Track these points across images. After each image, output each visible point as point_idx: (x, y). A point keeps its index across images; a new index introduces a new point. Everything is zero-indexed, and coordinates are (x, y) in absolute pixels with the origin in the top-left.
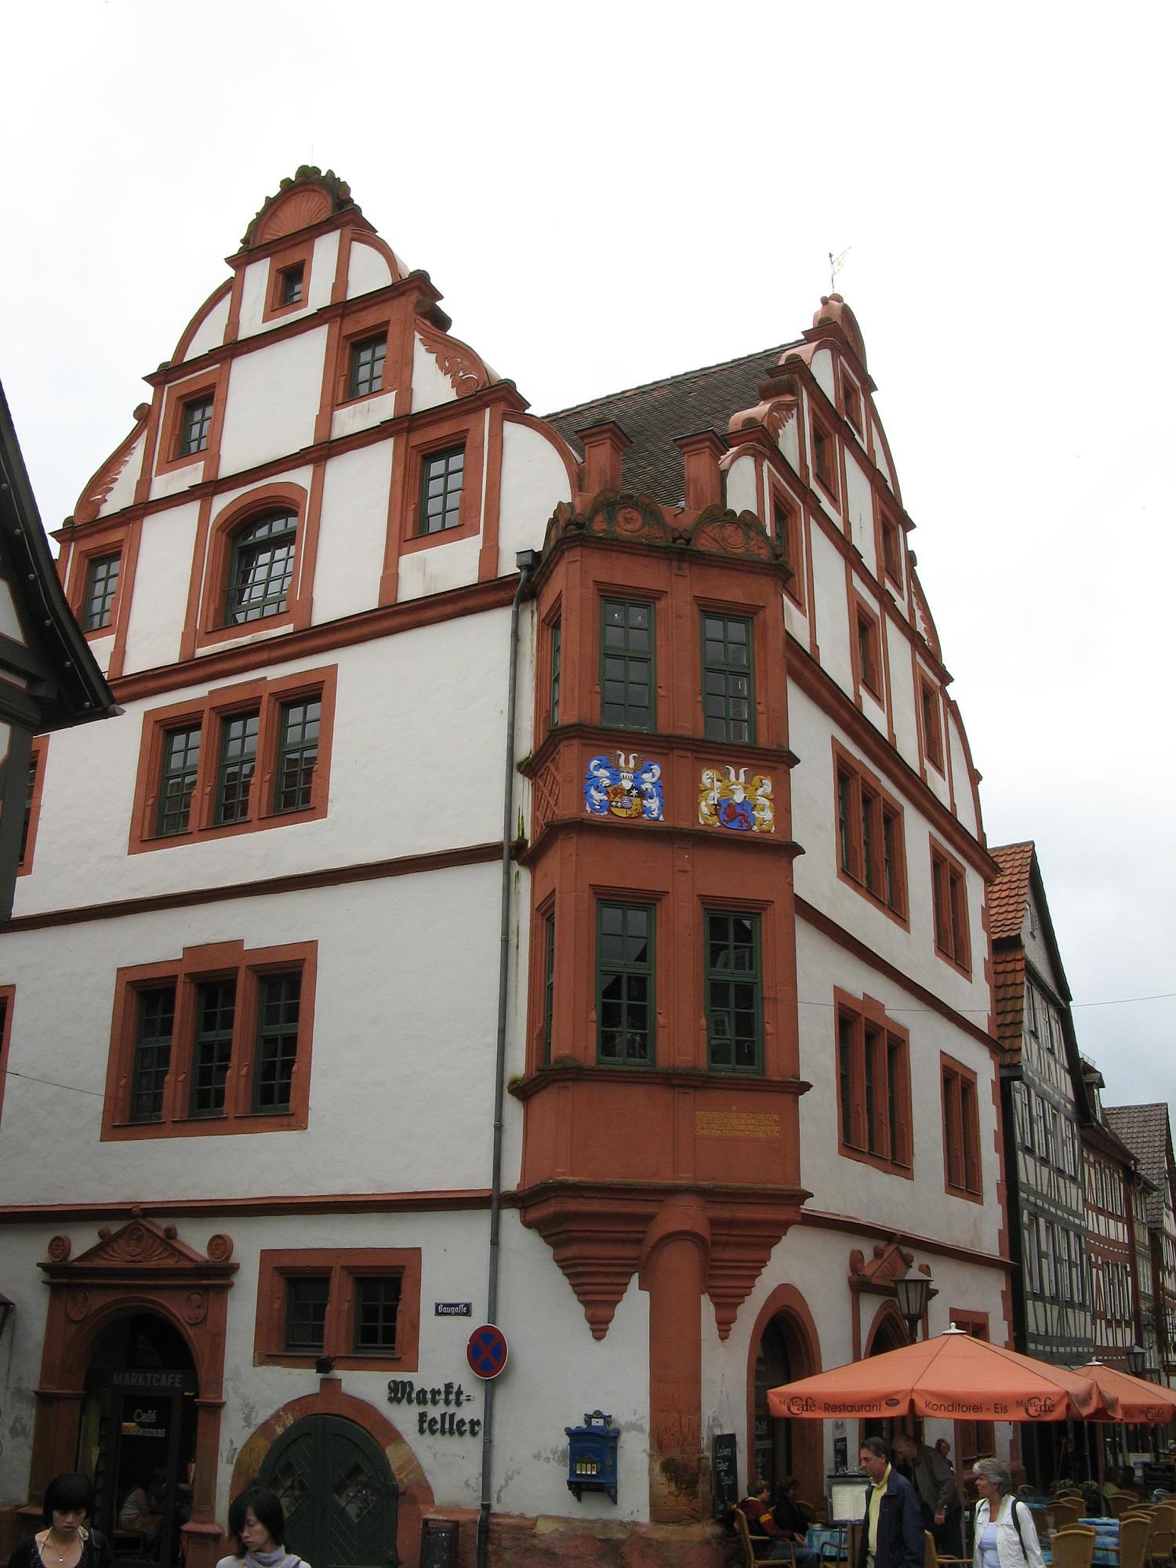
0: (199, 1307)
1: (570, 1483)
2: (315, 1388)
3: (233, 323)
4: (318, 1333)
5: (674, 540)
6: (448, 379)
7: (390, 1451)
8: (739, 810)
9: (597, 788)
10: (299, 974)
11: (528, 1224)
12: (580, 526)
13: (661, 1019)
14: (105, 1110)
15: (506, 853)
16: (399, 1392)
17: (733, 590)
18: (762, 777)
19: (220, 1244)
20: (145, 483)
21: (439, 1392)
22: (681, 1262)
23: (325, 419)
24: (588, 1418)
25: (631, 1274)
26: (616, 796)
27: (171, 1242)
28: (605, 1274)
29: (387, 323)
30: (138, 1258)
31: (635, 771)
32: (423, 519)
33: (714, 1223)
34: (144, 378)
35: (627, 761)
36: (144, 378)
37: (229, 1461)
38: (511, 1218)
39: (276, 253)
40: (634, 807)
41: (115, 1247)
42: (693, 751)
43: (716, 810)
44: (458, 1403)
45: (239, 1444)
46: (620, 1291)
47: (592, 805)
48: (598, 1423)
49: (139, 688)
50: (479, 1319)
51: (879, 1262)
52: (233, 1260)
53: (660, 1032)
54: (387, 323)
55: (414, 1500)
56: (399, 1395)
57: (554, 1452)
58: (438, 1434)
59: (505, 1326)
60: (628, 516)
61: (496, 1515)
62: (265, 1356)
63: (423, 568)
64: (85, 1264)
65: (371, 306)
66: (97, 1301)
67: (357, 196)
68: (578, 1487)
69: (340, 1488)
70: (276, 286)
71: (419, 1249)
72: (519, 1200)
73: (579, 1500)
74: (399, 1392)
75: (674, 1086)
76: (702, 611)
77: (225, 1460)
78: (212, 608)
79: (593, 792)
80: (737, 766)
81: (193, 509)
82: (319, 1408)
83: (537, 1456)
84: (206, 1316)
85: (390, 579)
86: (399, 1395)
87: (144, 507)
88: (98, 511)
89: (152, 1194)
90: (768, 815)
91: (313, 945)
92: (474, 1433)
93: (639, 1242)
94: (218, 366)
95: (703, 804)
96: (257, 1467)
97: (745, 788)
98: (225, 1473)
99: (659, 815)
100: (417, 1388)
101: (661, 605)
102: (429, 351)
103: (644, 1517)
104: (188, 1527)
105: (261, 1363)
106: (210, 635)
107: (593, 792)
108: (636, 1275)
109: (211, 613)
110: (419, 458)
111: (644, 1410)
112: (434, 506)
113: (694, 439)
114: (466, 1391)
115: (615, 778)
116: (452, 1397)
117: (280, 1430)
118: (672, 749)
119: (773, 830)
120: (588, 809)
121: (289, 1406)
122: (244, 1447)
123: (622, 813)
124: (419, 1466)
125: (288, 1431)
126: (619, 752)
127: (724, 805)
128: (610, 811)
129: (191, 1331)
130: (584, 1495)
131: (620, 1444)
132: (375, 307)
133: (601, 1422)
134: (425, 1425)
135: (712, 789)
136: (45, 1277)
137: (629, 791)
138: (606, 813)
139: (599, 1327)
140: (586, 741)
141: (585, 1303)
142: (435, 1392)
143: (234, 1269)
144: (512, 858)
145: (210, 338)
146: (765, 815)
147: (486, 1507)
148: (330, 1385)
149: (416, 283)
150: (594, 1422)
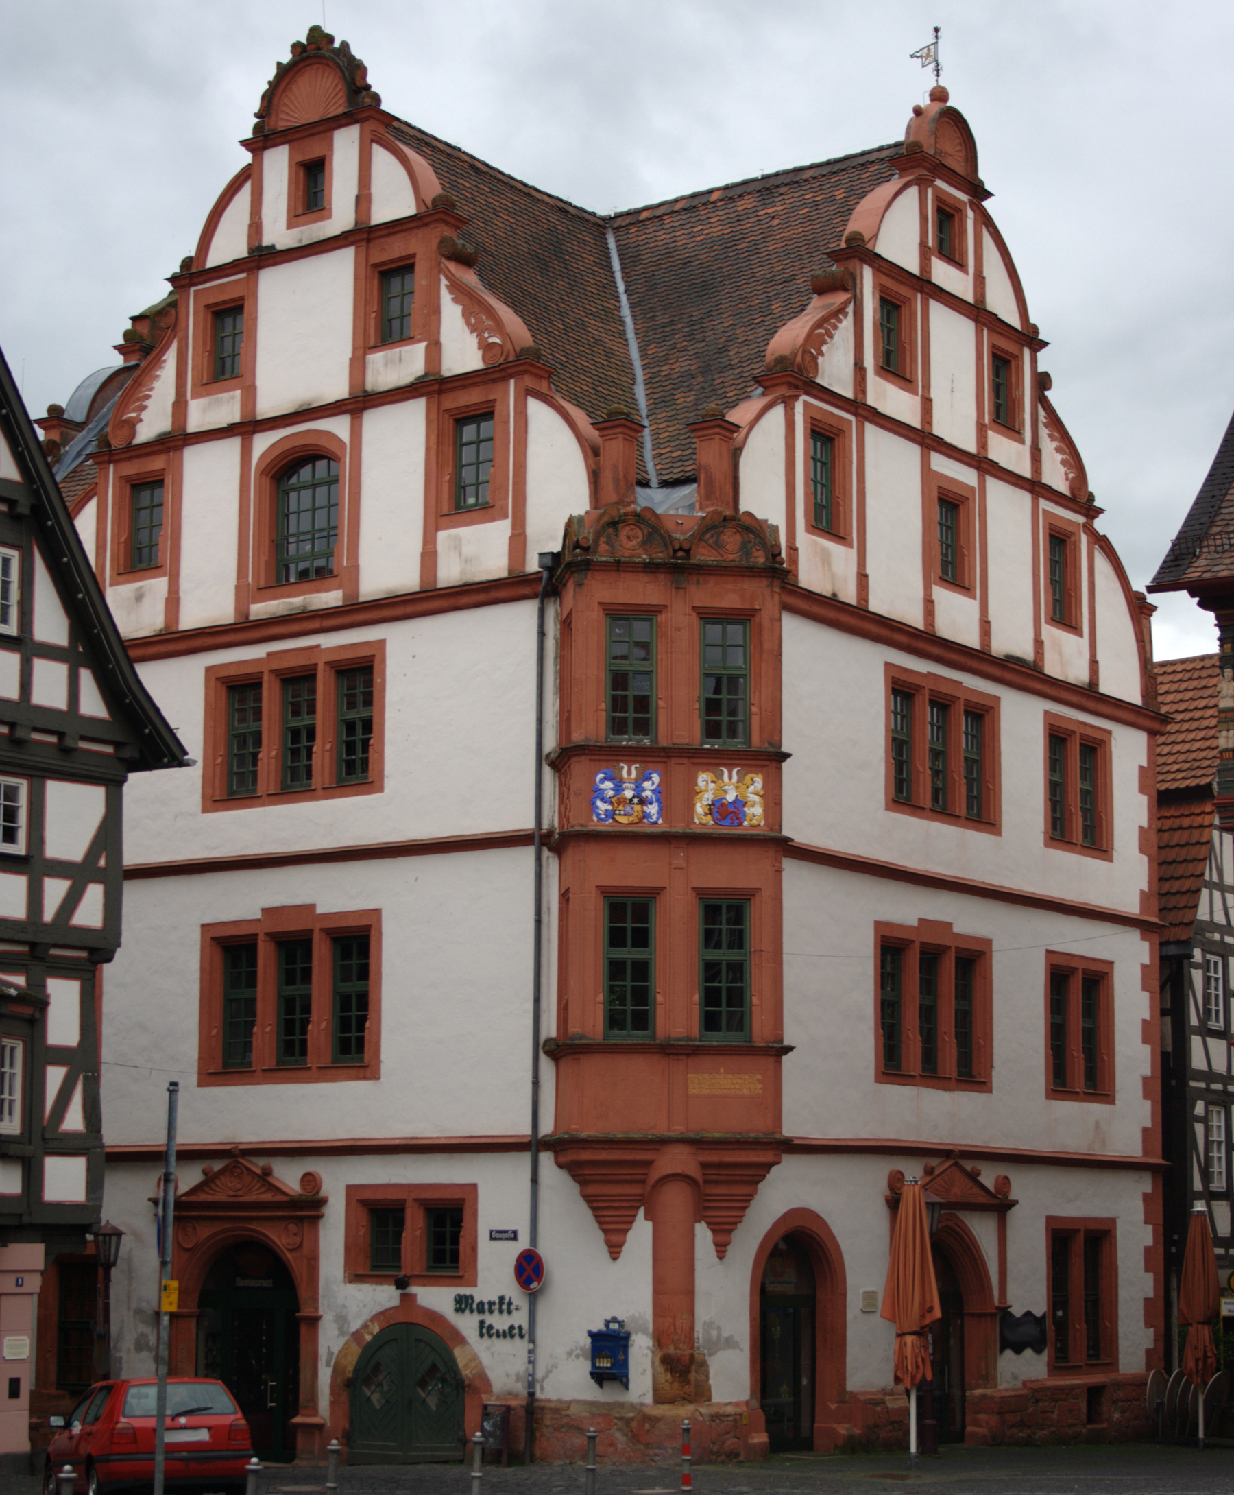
0: (295, 1234)
1: (593, 1374)
2: (395, 1302)
3: (255, 227)
4: (397, 1254)
7: (457, 1352)
8: (731, 809)
9: (602, 799)
11: (560, 1166)
12: (586, 549)
13: (659, 998)
14: (200, 1058)
15: (537, 840)
16: (463, 1304)
17: (729, 596)
18: (753, 775)
19: (310, 1180)
20: (180, 407)
21: (494, 1303)
22: (676, 1199)
25: (637, 1208)
26: (619, 804)
27: (270, 1179)
28: (616, 1208)
29: (414, 256)
30: (241, 1193)
31: (636, 781)
33: (704, 1166)
35: (629, 772)
37: (328, 1364)
38: (546, 1159)
40: (636, 814)
41: (218, 1182)
42: (689, 758)
43: (710, 809)
44: (509, 1312)
45: (336, 1350)
47: (598, 815)
49: (198, 642)
50: (523, 1244)
51: (928, 1179)
53: (658, 1007)
54: (414, 256)
55: (477, 1391)
56: (463, 1306)
57: (582, 1349)
58: (517, 1338)
59: (544, 1251)
60: (631, 533)
61: (538, 1400)
62: (355, 1276)
63: (457, 545)
64: (193, 1198)
65: (396, 233)
67: (374, 80)
68: (599, 1377)
69: (423, 1384)
70: (297, 182)
71: (474, 1186)
72: (555, 1145)
73: (601, 1387)
74: (463, 1304)
75: (669, 1054)
76: (701, 618)
77: (324, 1363)
79: (599, 803)
80: (730, 767)
82: (401, 1319)
83: (570, 1354)
84: (301, 1244)
85: (429, 557)
86: (463, 1306)
88: (133, 434)
91: (377, 912)
92: (522, 1336)
93: (643, 1182)
94: (243, 275)
95: (698, 805)
96: (351, 1368)
97: (737, 788)
98: (325, 1376)
99: (658, 819)
100: (477, 1300)
101: (662, 618)
102: (455, 300)
103: (649, 1399)
104: (297, 1419)
105: (350, 1282)
106: (264, 591)
107: (599, 803)
109: (263, 566)
110: (452, 421)
114: (515, 1302)
115: (618, 788)
116: (505, 1307)
117: (368, 1338)
118: (669, 757)
119: (762, 823)
120: (595, 818)
121: (376, 1317)
122: (340, 1352)
124: (480, 1363)
125: (376, 1338)
126: (622, 764)
127: (718, 805)
128: (613, 819)
129: (289, 1256)
130: (606, 1384)
131: (630, 1343)
132: (400, 235)
134: (486, 1330)
135: (706, 791)
137: (631, 800)
138: (611, 821)
139: (615, 1250)
140: (593, 757)
141: (605, 1231)
142: (491, 1304)
143: (323, 1202)
144: (542, 844)
146: (755, 811)
147: (531, 1395)
148: (407, 1299)
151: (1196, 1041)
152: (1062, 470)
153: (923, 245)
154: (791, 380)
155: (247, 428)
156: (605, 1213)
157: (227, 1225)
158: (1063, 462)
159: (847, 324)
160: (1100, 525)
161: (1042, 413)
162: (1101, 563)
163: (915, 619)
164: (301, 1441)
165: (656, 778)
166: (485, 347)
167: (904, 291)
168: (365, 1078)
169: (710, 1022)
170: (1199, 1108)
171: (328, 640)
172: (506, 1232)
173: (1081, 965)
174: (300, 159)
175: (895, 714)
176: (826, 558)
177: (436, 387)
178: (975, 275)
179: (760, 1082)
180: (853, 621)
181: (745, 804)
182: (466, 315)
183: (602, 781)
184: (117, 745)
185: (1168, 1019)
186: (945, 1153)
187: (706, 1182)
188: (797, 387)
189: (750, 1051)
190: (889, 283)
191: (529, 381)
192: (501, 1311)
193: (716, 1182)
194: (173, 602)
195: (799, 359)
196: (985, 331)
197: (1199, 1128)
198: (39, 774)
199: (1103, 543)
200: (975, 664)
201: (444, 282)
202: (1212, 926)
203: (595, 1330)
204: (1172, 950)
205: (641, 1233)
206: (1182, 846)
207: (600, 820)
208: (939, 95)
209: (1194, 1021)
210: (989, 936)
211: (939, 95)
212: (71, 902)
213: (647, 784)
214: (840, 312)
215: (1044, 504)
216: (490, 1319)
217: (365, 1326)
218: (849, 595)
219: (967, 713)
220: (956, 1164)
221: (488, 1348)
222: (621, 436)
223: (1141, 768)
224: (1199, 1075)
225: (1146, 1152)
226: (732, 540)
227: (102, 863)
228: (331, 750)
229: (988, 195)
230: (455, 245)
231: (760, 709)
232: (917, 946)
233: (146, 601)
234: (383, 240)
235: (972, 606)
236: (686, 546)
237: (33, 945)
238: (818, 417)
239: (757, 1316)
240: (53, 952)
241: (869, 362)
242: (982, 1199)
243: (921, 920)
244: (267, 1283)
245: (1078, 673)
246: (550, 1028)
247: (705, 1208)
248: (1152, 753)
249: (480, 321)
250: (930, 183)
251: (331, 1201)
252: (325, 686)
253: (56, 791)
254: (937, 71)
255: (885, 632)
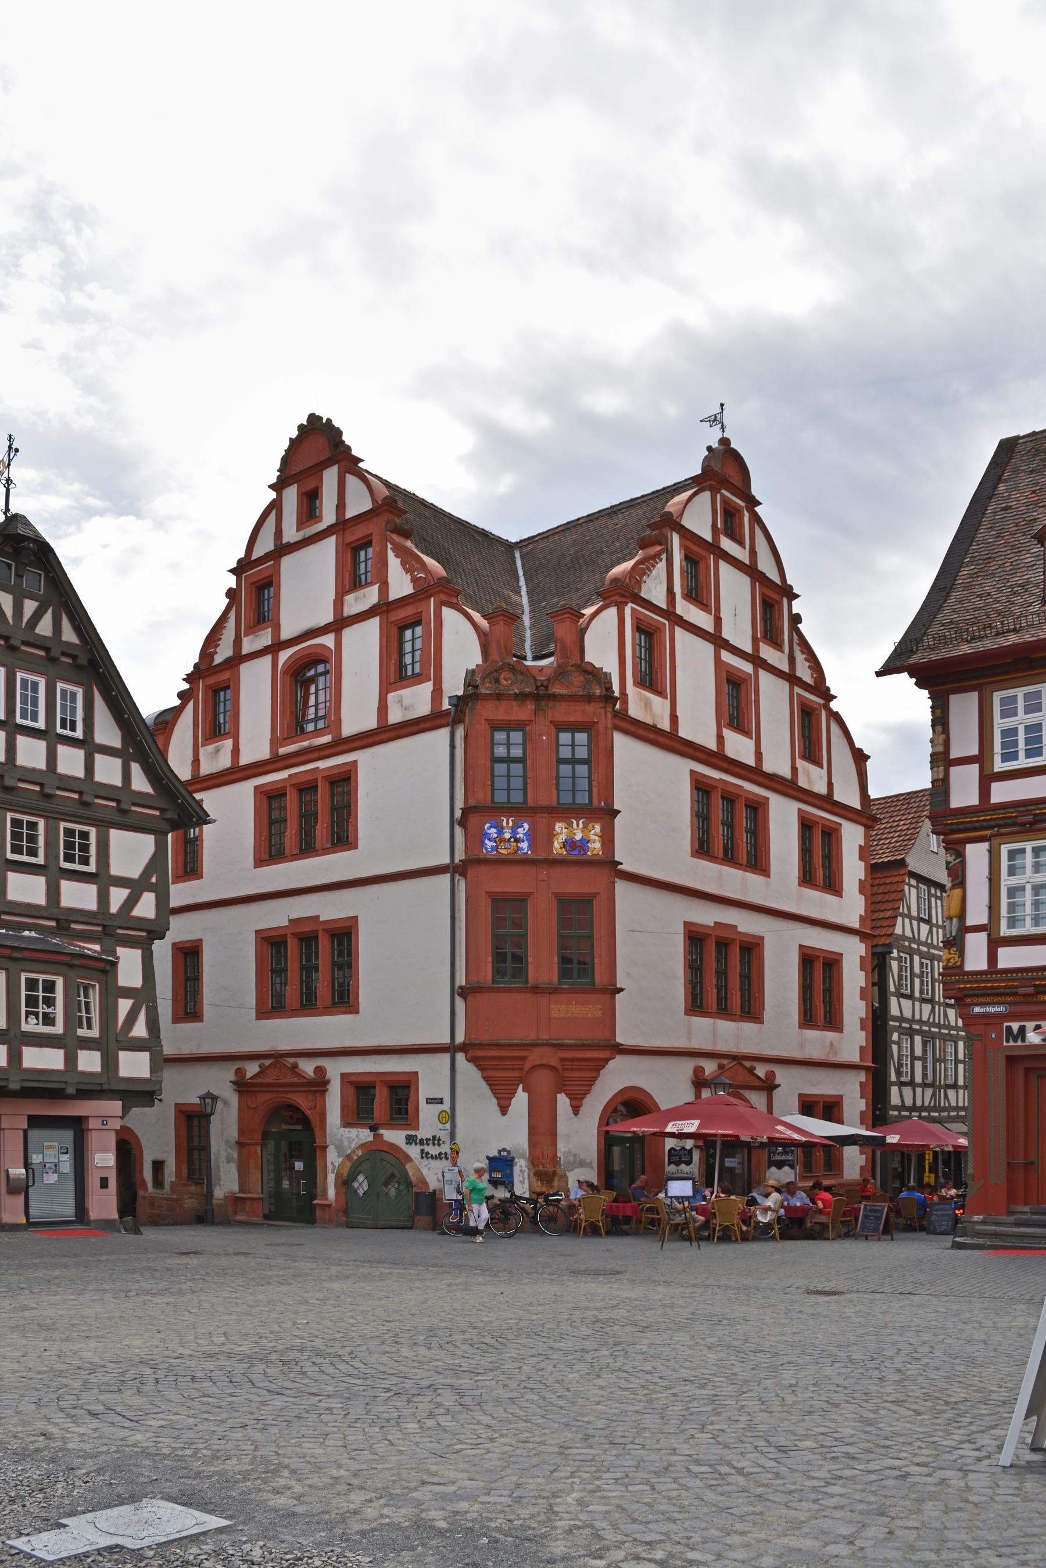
2: (371, 1138)
3: (279, 533)
5: (537, 687)
6: (408, 577)
8: (579, 844)
9: (489, 839)
10: (351, 933)
11: (469, 1060)
15: (451, 869)
16: (411, 1140)
19: (320, 1070)
20: (238, 642)
21: (430, 1140)
22: (544, 1080)
23: (338, 604)
24: (500, 1152)
25: (519, 1085)
26: (501, 842)
27: (296, 1070)
29: (371, 534)
31: (512, 828)
32: (401, 666)
33: (562, 1060)
34: (230, 571)
35: (507, 822)
36: (230, 571)
37: (333, 1172)
38: (460, 1057)
39: (300, 480)
42: (549, 813)
44: (439, 1145)
45: (337, 1165)
46: (513, 1093)
48: (504, 1154)
49: (249, 772)
51: (721, 1071)
52: (327, 1078)
54: (371, 534)
58: (444, 1159)
62: (347, 1122)
65: (360, 523)
66: (262, 1098)
69: (386, 1184)
72: (464, 1048)
74: (411, 1140)
78: (285, 723)
79: (487, 841)
81: (268, 659)
85: (383, 709)
87: (238, 659)
88: (212, 660)
89: (284, 1046)
90: (598, 845)
92: (447, 1158)
93: (521, 1069)
97: (582, 831)
98: (331, 1178)
100: (419, 1138)
102: (397, 556)
105: (344, 1127)
107: (487, 841)
108: (521, 1086)
111: (525, 1145)
112: (408, 659)
113: (559, 613)
114: (443, 1139)
116: (436, 1142)
117: (355, 1158)
118: (535, 813)
119: (601, 853)
120: (484, 851)
123: (504, 852)
125: (359, 1158)
132: (362, 524)
133: (506, 1154)
134: (424, 1155)
135: (561, 833)
136: (235, 1087)
137: (509, 839)
139: (504, 1110)
142: (428, 1140)
143: (328, 1082)
145: (265, 545)
146: (596, 846)
148: (378, 1137)
149: (386, 508)
150: (502, 1153)
151: (893, 1001)
152: (810, 672)
153: (714, 526)
154: (623, 592)
155: (275, 648)
156: (499, 1087)
157: (273, 1095)
158: (809, 667)
159: (662, 565)
160: (834, 705)
161: (795, 637)
162: (835, 728)
163: (712, 745)
164: (318, 1213)
165: (526, 826)
166: (415, 580)
167: (701, 551)
168: (350, 1013)
169: (565, 974)
170: (895, 1036)
171: (323, 764)
172: (436, 1099)
173: (822, 955)
174: (304, 490)
175: (698, 802)
176: (648, 705)
177: (385, 608)
178: (750, 549)
179: (600, 1009)
180: (667, 742)
181: (588, 841)
182: (403, 564)
183: (489, 828)
184: (162, 810)
185: (876, 988)
186: (734, 1057)
187: (563, 1069)
188: (625, 597)
189: (593, 990)
190: (691, 545)
191: (443, 597)
192: (434, 1144)
193: (572, 1070)
194: (236, 752)
195: (627, 580)
196: (757, 584)
197: (895, 1047)
198: (104, 825)
199: (837, 717)
200: (752, 776)
201: (389, 546)
202: (904, 937)
203: (491, 1155)
204: (879, 950)
205: (521, 1099)
206: (886, 893)
207: (487, 851)
208: (725, 442)
209: (892, 989)
210: (761, 934)
211: (725, 442)
212: (131, 902)
213: (520, 830)
214: (656, 557)
215: (797, 690)
216: (427, 1149)
217: (354, 1152)
218: (666, 726)
219: (747, 806)
220: (740, 1064)
221: (426, 1166)
222: (502, 622)
223: (860, 846)
224: (895, 1019)
225: (862, 1059)
226: (577, 679)
227: (154, 880)
228: (327, 827)
229: (759, 503)
230: (395, 523)
231: (599, 783)
232: (714, 937)
233: (221, 752)
234: (352, 529)
235: (751, 744)
236: (545, 684)
237: (104, 926)
238: (642, 618)
239: (602, 1147)
240: (119, 931)
241: (677, 589)
242: (757, 1083)
243: (715, 923)
244: (300, 1127)
245: (821, 789)
246: (461, 980)
247: (563, 1085)
248: (867, 837)
249: (411, 566)
250: (719, 492)
251: (332, 1082)
252: (323, 792)
253: (116, 837)
254: (723, 428)
255: (690, 751)
